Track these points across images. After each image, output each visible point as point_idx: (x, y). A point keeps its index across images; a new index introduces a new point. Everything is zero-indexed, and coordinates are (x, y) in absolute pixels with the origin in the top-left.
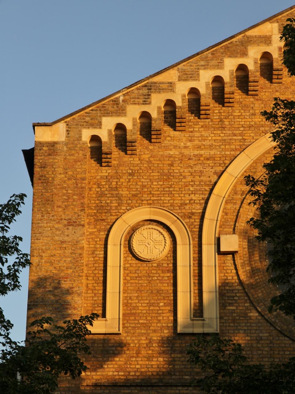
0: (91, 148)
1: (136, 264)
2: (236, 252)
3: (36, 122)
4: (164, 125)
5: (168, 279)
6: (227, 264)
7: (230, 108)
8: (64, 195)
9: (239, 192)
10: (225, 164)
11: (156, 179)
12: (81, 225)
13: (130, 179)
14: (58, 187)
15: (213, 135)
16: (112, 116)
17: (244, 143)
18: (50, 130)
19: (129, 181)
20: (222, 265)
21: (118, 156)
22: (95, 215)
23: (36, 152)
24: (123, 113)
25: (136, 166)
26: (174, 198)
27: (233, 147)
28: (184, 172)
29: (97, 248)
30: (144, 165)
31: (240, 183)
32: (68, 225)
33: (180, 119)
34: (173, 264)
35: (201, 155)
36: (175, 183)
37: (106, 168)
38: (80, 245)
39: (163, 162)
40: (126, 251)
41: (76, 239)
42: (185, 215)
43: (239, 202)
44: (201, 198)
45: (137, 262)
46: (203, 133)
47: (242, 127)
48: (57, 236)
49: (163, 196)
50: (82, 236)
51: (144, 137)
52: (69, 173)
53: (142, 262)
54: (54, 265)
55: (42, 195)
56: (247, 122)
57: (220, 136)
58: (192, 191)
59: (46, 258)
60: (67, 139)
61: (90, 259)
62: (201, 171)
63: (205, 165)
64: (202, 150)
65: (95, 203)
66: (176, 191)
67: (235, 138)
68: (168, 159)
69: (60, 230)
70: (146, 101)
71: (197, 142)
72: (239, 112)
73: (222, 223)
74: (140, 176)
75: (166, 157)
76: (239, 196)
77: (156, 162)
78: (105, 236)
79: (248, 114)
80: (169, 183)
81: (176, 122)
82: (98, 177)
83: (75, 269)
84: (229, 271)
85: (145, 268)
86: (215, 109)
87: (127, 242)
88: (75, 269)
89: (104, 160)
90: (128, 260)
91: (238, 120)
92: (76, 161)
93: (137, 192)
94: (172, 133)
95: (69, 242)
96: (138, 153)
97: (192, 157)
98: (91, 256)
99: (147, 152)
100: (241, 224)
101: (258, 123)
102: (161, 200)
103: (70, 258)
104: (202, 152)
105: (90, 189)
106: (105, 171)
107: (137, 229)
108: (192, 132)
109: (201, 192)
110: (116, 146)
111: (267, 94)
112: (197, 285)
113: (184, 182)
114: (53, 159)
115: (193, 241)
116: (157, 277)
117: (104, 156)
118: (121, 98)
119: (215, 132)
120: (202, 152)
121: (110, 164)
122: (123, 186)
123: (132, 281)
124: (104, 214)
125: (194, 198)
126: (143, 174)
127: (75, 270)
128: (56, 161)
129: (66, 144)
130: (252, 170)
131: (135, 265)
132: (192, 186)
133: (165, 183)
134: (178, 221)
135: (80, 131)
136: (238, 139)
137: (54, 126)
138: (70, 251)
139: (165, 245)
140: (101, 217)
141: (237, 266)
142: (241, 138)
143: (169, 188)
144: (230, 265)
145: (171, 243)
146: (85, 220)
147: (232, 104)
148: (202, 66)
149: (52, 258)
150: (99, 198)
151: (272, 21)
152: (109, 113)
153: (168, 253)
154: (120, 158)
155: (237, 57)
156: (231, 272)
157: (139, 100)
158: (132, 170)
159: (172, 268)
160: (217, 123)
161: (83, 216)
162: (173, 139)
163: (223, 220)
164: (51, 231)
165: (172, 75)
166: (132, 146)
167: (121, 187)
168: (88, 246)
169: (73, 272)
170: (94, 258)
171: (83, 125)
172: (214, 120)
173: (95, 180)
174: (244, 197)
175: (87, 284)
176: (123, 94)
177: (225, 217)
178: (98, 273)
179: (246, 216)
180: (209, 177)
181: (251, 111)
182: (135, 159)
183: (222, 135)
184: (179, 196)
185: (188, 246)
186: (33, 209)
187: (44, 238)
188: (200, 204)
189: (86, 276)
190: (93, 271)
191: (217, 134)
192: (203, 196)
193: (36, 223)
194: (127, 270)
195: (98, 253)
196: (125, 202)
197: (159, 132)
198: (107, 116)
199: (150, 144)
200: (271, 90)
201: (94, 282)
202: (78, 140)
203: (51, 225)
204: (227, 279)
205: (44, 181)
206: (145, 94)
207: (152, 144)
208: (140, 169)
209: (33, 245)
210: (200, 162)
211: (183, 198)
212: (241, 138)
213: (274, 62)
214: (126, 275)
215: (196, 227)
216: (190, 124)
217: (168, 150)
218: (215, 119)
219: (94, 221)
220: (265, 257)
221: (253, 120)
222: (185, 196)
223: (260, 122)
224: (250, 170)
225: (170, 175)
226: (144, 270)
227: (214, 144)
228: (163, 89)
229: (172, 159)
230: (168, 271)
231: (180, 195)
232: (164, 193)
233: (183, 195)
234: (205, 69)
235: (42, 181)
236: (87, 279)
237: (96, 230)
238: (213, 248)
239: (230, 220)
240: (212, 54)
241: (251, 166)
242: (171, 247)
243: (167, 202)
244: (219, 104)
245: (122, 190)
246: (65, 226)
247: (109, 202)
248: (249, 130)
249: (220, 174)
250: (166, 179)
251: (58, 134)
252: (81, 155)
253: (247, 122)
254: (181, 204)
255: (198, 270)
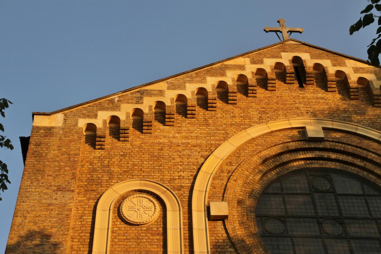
0: (86, 135)
1: (125, 228)
2: (226, 217)
3: (36, 111)
4: (155, 121)
5: (158, 242)
6: (218, 229)
7: (213, 112)
8: (56, 166)
9: (225, 171)
10: (211, 150)
11: (147, 160)
12: (70, 191)
13: (121, 159)
14: (51, 160)
15: (199, 130)
16: (107, 110)
17: (227, 136)
18: (49, 119)
19: (121, 160)
20: (213, 230)
21: (111, 142)
22: (86, 186)
23: (31, 140)
24: (117, 109)
25: (128, 150)
26: (164, 174)
27: (218, 138)
28: (173, 155)
29: (85, 214)
30: (136, 149)
31: (225, 164)
32: (57, 191)
33: (169, 115)
34: (163, 228)
35: (189, 143)
36: (164, 163)
37: (99, 151)
38: (68, 207)
39: (153, 147)
40: (115, 217)
41: (65, 202)
42: (175, 188)
43: (226, 179)
44: (190, 175)
45: (126, 226)
46: (190, 128)
47: (225, 124)
48: (45, 199)
49: (153, 173)
50: (70, 200)
51: (136, 129)
52: (63, 150)
53: (131, 226)
54: (38, 225)
55: (34, 166)
56: (228, 121)
57: (205, 130)
58: (181, 169)
59: (30, 218)
60: (64, 125)
61: (77, 223)
62: (188, 155)
63: (193, 150)
64: (189, 139)
65: (86, 177)
66: (166, 169)
67: (219, 132)
68: (158, 145)
69: (48, 195)
70: (139, 100)
71: (184, 134)
72: (221, 115)
73: (210, 195)
74: (132, 157)
75: (156, 144)
76: (226, 174)
77: (147, 147)
78: (94, 204)
79: (229, 116)
80: (159, 163)
81: (165, 118)
82: (91, 157)
83: (60, 228)
84: (220, 235)
85: (134, 232)
86: (200, 112)
87: (116, 209)
88: (60, 228)
89: (97, 143)
90: (117, 225)
91: (220, 120)
92: (70, 141)
93: (128, 169)
94: (162, 127)
95: (57, 204)
96: (130, 141)
97: (180, 144)
98: (78, 220)
99: (138, 140)
100: (229, 196)
101: (239, 122)
102: (151, 175)
103: (55, 218)
104: (190, 141)
105: (83, 166)
106: (98, 153)
107: (126, 198)
108: (179, 127)
109: (190, 170)
110: (110, 135)
111: (244, 104)
112: (188, 247)
113: (173, 162)
114: (48, 139)
115: (183, 209)
116: (146, 239)
117: (97, 139)
118: (116, 99)
119: (200, 127)
120: (190, 141)
121: (103, 147)
122: (115, 165)
123: (119, 243)
124: (94, 186)
125: (182, 175)
126: (134, 156)
127: (60, 229)
128: (51, 141)
129: (63, 129)
130: (236, 155)
131: (123, 229)
132: (181, 165)
133: (155, 163)
134: (168, 191)
135: (77, 120)
136: (221, 133)
137: (53, 116)
138: (57, 212)
139: (155, 211)
140: (92, 188)
141: (228, 230)
142: (224, 132)
143: (159, 167)
144: (221, 230)
145: (161, 210)
146: (74, 186)
147: (214, 109)
148: (188, 81)
149: (36, 218)
150: (91, 173)
151: (244, 57)
152: (105, 109)
153: (158, 219)
154: (112, 143)
155: (217, 76)
156: (222, 236)
157: (132, 101)
158: (124, 152)
159: (162, 232)
160: (202, 121)
161: (73, 183)
162: (162, 131)
163: (211, 192)
164: (39, 196)
165: (163, 86)
166: (125, 133)
167: (113, 165)
168: (76, 212)
169: (57, 231)
170: (81, 222)
171: (80, 116)
172: (199, 119)
173: (87, 159)
174: (230, 174)
175: (72, 245)
176: (118, 97)
177: (213, 190)
178: (85, 236)
179: (233, 190)
180: (197, 159)
181: (232, 115)
182: (127, 145)
183: (206, 130)
184: (169, 173)
185: (178, 212)
186: (22, 177)
187: (31, 201)
188: (189, 179)
189: (72, 238)
190: (79, 233)
191: (203, 129)
192: (192, 173)
193: (24, 189)
194: (116, 233)
195: (86, 217)
196: (116, 176)
197: (150, 124)
198: (103, 110)
199: (141, 134)
200: (247, 102)
201: (79, 243)
202: (74, 126)
203: (39, 190)
204: (218, 242)
205: (37, 155)
206: (137, 97)
207: (143, 134)
208: (132, 152)
209: (18, 207)
210: (188, 148)
211: (172, 175)
212: (224, 132)
213: (248, 80)
214: (114, 237)
215: (185, 197)
216: (178, 121)
217: (158, 139)
218: (200, 119)
219: (84, 191)
220: (254, 227)
221: (234, 120)
222: (175, 173)
223: (240, 122)
224: (234, 155)
225: (160, 157)
226: (133, 233)
227: (200, 135)
228: (154, 94)
229: (162, 145)
230: (158, 234)
231: (169, 172)
232: (154, 170)
233: (172, 172)
234: (190, 83)
235: (35, 155)
236: (73, 241)
237: (85, 198)
238: (203, 214)
239: (218, 192)
240: (196, 74)
241: (235, 152)
242: (160, 214)
243: (157, 177)
244: (204, 109)
245: (114, 167)
246: (54, 191)
247: (100, 176)
248: (231, 127)
249: (206, 157)
250: (156, 160)
251: (57, 121)
252: (76, 137)
253: (228, 121)
254: (171, 179)
255: (188, 233)
